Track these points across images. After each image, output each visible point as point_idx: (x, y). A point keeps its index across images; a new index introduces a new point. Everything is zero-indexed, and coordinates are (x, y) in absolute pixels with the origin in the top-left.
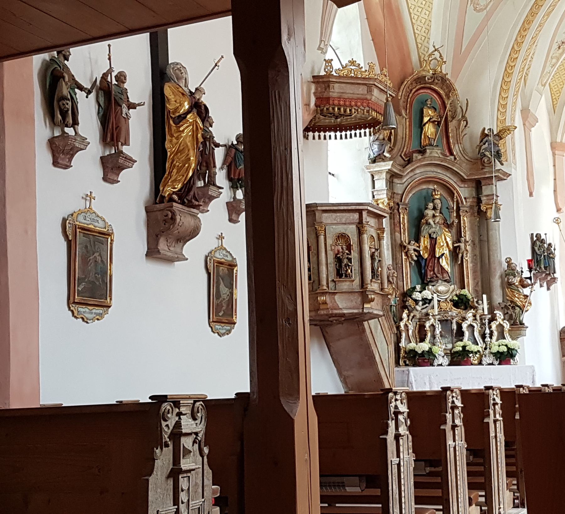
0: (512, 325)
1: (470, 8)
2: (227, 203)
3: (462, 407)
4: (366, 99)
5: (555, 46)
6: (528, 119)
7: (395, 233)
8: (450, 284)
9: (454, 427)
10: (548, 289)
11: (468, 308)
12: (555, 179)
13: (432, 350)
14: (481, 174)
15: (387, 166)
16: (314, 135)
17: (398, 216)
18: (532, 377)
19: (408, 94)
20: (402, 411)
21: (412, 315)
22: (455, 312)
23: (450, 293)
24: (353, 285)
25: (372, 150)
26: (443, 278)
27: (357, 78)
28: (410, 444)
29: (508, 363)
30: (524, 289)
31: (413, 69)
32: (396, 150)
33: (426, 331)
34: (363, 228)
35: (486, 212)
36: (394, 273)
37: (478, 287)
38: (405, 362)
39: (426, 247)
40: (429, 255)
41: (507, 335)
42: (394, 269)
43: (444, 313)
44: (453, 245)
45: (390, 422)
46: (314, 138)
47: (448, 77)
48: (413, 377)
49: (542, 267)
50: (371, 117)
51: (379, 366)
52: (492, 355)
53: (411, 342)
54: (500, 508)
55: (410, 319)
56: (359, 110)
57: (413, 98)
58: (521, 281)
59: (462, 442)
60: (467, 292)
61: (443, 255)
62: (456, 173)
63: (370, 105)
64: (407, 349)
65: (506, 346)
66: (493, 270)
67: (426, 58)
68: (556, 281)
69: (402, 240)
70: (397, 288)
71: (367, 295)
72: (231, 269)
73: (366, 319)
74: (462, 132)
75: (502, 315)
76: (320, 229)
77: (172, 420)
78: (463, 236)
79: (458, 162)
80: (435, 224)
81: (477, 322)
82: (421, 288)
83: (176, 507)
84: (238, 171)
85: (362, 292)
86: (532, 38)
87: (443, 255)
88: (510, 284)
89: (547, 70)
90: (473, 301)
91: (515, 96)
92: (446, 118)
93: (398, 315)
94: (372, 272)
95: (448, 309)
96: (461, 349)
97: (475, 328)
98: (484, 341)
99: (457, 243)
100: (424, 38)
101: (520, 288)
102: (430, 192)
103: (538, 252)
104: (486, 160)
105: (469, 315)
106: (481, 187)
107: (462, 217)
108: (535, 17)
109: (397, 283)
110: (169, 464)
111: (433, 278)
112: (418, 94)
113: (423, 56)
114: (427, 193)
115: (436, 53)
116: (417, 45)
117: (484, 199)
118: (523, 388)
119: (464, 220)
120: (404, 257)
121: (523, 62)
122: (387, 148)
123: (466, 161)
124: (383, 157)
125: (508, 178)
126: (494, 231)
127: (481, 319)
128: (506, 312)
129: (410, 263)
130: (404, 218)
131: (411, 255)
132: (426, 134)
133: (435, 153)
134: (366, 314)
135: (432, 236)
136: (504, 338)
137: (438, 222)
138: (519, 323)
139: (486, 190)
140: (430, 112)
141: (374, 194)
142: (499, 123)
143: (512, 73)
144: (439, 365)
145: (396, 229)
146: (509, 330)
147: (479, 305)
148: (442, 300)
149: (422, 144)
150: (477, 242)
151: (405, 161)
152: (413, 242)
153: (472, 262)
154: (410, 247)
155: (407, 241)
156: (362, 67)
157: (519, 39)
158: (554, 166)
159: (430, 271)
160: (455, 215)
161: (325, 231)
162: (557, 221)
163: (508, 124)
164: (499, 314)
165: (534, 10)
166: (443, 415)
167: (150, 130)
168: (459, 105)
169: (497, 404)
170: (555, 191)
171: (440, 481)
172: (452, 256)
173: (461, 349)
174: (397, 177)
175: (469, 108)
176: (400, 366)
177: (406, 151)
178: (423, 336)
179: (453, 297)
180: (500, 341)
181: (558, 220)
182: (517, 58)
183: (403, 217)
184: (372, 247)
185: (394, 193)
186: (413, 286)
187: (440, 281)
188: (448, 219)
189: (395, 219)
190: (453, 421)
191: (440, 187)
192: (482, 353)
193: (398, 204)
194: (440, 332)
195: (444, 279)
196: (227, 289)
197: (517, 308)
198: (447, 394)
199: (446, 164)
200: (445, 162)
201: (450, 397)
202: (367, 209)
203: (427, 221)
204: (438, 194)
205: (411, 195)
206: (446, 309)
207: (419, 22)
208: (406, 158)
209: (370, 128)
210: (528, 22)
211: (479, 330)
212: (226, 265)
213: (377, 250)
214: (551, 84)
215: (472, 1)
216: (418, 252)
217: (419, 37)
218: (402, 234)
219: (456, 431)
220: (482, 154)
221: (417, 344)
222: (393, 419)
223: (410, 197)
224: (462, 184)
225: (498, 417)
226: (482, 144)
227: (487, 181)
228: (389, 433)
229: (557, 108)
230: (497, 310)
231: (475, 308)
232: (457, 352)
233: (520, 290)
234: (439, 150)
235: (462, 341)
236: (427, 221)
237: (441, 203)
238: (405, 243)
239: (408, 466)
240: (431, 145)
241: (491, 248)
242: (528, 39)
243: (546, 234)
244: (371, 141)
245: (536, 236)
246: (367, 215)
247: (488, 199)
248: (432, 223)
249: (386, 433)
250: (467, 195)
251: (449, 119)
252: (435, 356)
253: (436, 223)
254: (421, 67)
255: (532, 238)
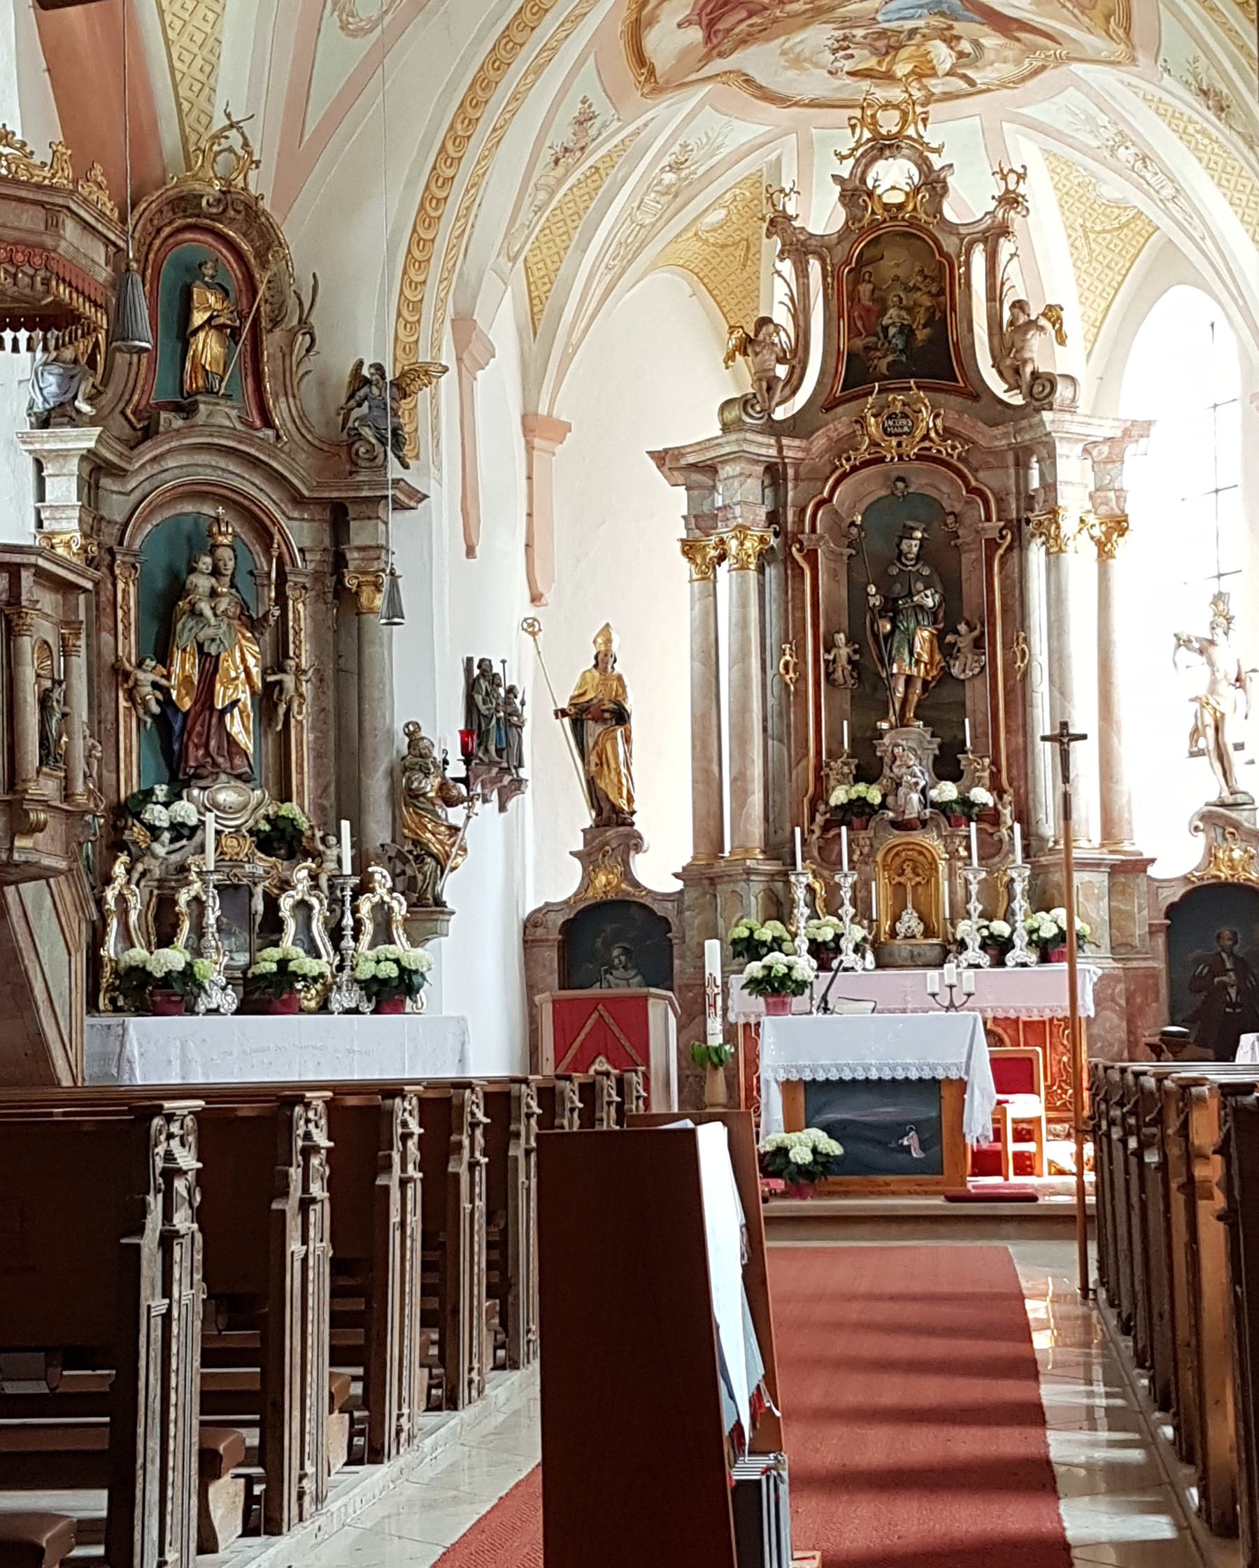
0: (414, 905)
1: (331, 21)
4: (44, 248)
5: (546, 156)
7: (99, 630)
8: (251, 785)
9: (306, 1204)
10: (502, 808)
11: (299, 856)
12: (530, 515)
13: (196, 969)
14: (349, 487)
15: (85, 439)
17: (110, 586)
18: (458, 1047)
19: (149, 240)
20: (185, 1168)
21: (140, 867)
22: (261, 864)
23: (249, 812)
25: (41, 389)
26: (232, 768)
27: (16, 182)
28: (199, 1257)
29: (398, 1009)
30: (449, 810)
31: (164, 171)
32: (109, 394)
33: (177, 915)
34: (20, 617)
35: (357, 593)
36: (94, 747)
38: (113, 1001)
39: (187, 679)
40: (195, 704)
41: (398, 933)
42: (92, 736)
43: (233, 867)
44: (263, 680)
45: (150, 1198)
47: (266, 205)
48: (135, 1044)
49: (492, 749)
50: (50, 299)
51: (41, 1012)
52: (356, 987)
53: (133, 946)
54: (400, 1416)
55: (134, 880)
56: (20, 275)
57: (161, 255)
58: (443, 787)
59: (324, 1244)
60: (297, 810)
61: (235, 703)
62: (277, 479)
63: (53, 264)
64: (122, 965)
65: (397, 961)
66: (369, 752)
67: (204, 144)
68: (523, 788)
69: (120, 654)
70: (100, 790)
71: (26, 813)
73: (12, 878)
74: (298, 364)
75: (389, 878)
78: (291, 654)
79: (286, 448)
80: (215, 615)
81: (322, 895)
82: (168, 794)
85: (9, 803)
86: (495, 130)
88: (414, 796)
89: (525, 215)
90: (314, 835)
91: (445, 283)
92: (256, 321)
93: (98, 866)
94: (41, 745)
95: (242, 856)
96: (274, 967)
97: (316, 911)
98: (337, 948)
99: (274, 673)
100: (200, 85)
101: (441, 807)
102: (204, 524)
103: (483, 708)
104: (362, 450)
105: (301, 875)
106: (348, 524)
107: (291, 602)
108: (505, 72)
109: (100, 776)
111: (204, 766)
112: (178, 244)
113: (193, 138)
114: (196, 524)
116: (179, 105)
117: (353, 557)
118: (473, 1090)
119: (296, 611)
120: (123, 703)
121: (467, 191)
122: (85, 388)
124: (74, 414)
125: (420, 505)
126: (377, 648)
127: (331, 887)
128: (398, 871)
129: (139, 719)
130: (128, 593)
131: (143, 699)
132: (197, 361)
134: (17, 866)
135: (206, 650)
136: (392, 942)
137: (225, 612)
138: (431, 902)
139: (360, 534)
140: (212, 300)
141: (43, 516)
142: (399, 353)
143: (439, 218)
144: (209, 1012)
145: (103, 619)
146: (406, 920)
147: (328, 847)
148: (227, 830)
149: (187, 386)
150: (329, 673)
151: (134, 428)
152: (150, 663)
153: (313, 728)
154: (141, 675)
155: (133, 659)
156: (32, 153)
157: (459, 126)
158: (529, 478)
159: (197, 747)
160: (273, 594)
162: (531, 627)
163: (424, 357)
164: (380, 875)
165: (503, 53)
166: (279, 1172)
168: (293, 288)
169: (411, 1135)
170: (527, 545)
171: (258, 1345)
172: (260, 709)
173: (274, 967)
174: (110, 474)
175: (318, 299)
176: (98, 1011)
177: (139, 401)
178: (168, 930)
179: (257, 822)
180: (380, 947)
181: (533, 625)
182: (453, 178)
183: (124, 591)
184: (42, 672)
185: (102, 518)
186: (143, 788)
187: (223, 777)
189: (102, 593)
190: (306, 1189)
191: (232, 513)
192: (330, 979)
193: (111, 552)
194: (218, 919)
195: (235, 772)
197: (429, 860)
198: (295, 1114)
199: (252, 451)
200: (252, 446)
201: (302, 1122)
202: (36, 566)
205: (150, 527)
206: (238, 854)
207: (185, 40)
208: (139, 421)
209: (46, 331)
210: (483, 85)
211: (325, 917)
213: (60, 683)
214: (531, 260)
215: (335, 4)
216: (166, 691)
217: (187, 82)
218: (121, 638)
219: (312, 1214)
220: (353, 433)
221: (151, 953)
222: (159, 1191)
223: (146, 531)
224: (294, 509)
225: (411, 1171)
226: (352, 403)
228: (148, 1231)
229: (542, 322)
230: (377, 864)
231: (317, 856)
232: (263, 977)
233: (439, 811)
234: (233, 408)
235: (276, 944)
236: (193, 605)
237: (236, 557)
238: (127, 666)
239: (190, 1319)
240: (212, 392)
241: (367, 693)
242: (482, 132)
243: (504, 662)
244: (38, 362)
245: (479, 667)
246: (35, 582)
247: (363, 559)
248: (208, 612)
249: (140, 1230)
250: (307, 543)
251: (263, 324)
252: (201, 987)
253: (218, 612)
254: (189, 168)
255: (468, 670)
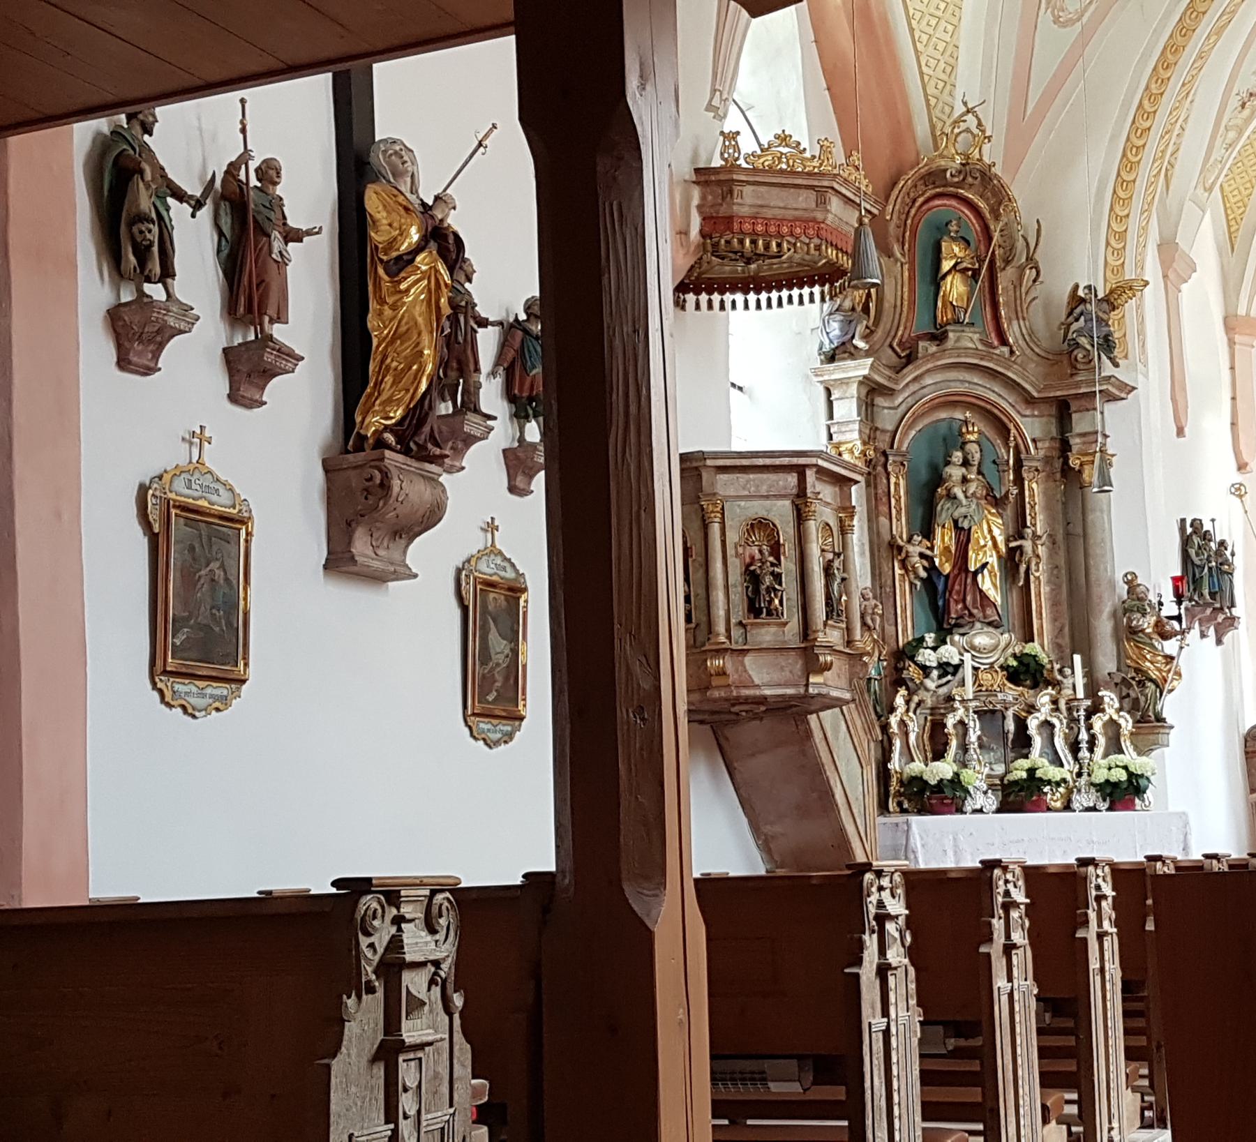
0: (1139, 722)
1: (1045, 17)
2: (504, 451)
3: (1026, 905)
4: (814, 220)
5: (1234, 102)
6: (1175, 265)
7: (877, 517)
8: (1000, 630)
9: (1009, 948)
10: (1219, 642)
11: (1041, 685)
12: (1233, 399)
13: (961, 778)
14: (1069, 387)
15: (860, 368)
16: (697, 300)
17: (885, 481)
18: (1182, 837)
19: (907, 209)
20: (893, 914)
21: (916, 699)
22: (1011, 692)
23: (999, 652)
24: (784, 632)
25: (827, 333)
26: (985, 618)
27: (794, 173)
28: (913, 986)
29: (1129, 806)
30: (1165, 643)
31: (918, 154)
32: (879, 333)
33: (946, 735)
34: (806, 506)
35: (1080, 472)
36: (876, 606)
37: (1063, 637)
38: (900, 804)
39: (947, 549)
40: (954, 567)
41: (1126, 744)
42: (875, 598)
43: (988, 696)
44: (1007, 545)
45: (866, 937)
46: (698, 307)
47: (997, 170)
48: (917, 837)
49: (1206, 592)
50: (824, 261)
51: (842, 813)
52: (1093, 790)
53: (913, 760)
54: (1110, 1129)
55: (912, 710)
56: (798, 244)
57: (917, 218)
58: (1159, 624)
59: (1028, 983)
60: (1038, 648)
61: (984, 565)
62: (1013, 385)
63: (823, 233)
64: (905, 776)
65: (1126, 768)
66: (1095, 599)
67: (948, 130)
68: (1236, 624)
69: (894, 532)
70: (883, 640)
71: (817, 655)
72: (514, 598)
73: (813, 708)
74: (1027, 293)
75: (1116, 700)
76: (711, 508)
77: (383, 934)
78: (1028, 524)
79: (1019, 361)
80: (966, 497)
81: (1061, 716)
82: (936, 640)
83: (392, 1126)
84: (528, 380)
85: (805, 648)
86: (1183, 85)
87: (984, 565)
88: (1133, 632)
89: (1215, 155)
90: (1053, 668)
91: (1146, 214)
92: (992, 262)
93: (884, 699)
94: (827, 604)
95: (995, 687)
96: (1024, 775)
97: (1057, 730)
98: (1076, 759)
99: (1016, 540)
100: (942, 84)
101: (1157, 640)
102: (956, 425)
103: (1196, 560)
104: (1080, 356)
105: (1044, 699)
106: (1070, 416)
107: (1026, 483)
108: (1190, 37)
109: (883, 629)
110: (375, 1031)
111: (962, 617)
112: (929, 209)
113: (939, 125)
114: (950, 428)
115: (970, 117)
116: (927, 101)
117: (1075, 442)
118: (1164, 862)
119: (1031, 489)
120: (898, 571)
121: (1162, 137)
122: (860, 329)
123: (1035, 358)
124: (852, 350)
125: (1129, 396)
126: (1098, 514)
127: (1069, 709)
128: (1124, 694)
129: (911, 584)
130: (899, 485)
131: (913, 567)
132: (946, 298)
133: (967, 340)
134: (813, 697)
135: (960, 525)
136: (1121, 751)
137: (974, 494)
138: (1153, 718)
139: (1080, 423)
140: (956, 249)
141: (832, 431)
142: (1109, 274)
143: (1139, 162)
144: (975, 811)
145: (880, 508)
146: (1132, 734)
147: (1065, 677)
148: (982, 667)
149: (939, 320)
150: (1060, 537)
151: (899, 357)
152: (917, 538)
153: (1049, 582)
154: (911, 548)
155: (905, 536)
156: (805, 149)
157: (1153, 86)
158: (1232, 368)
159: (957, 602)
160: (1011, 477)
161: (723, 514)
162: (1238, 491)
163: (1129, 275)
164: (1109, 698)
165: (1188, 21)
166: (984, 921)
167: (335, 290)
168: (1020, 233)
169: (1105, 897)
170: (1233, 424)
172: (1005, 568)
173: (1024, 775)
174: (882, 394)
175: (1042, 239)
176: (889, 812)
177: (902, 336)
178: (941, 747)
179: (1006, 659)
180: (1111, 757)
181: (1239, 489)
182: (1149, 129)
183: (895, 483)
184: (826, 548)
185: (877, 429)
186: (917, 636)
187: (978, 625)
188: (995, 486)
189: (879, 487)
190: (1008, 936)
191: (977, 416)
192: (1071, 784)
193: (885, 454)
194: (979, 738)
195: (987, 621)
196: (505, 642)
197: (1149, 684)
198: (994, 876)
199: (991, 365)
200: (989, 361)
201: (1001, 883)
202: (816, 465)
203: (949, 490)
204: (973, 432)
205: (914, 432)
206: (992, 685)
207: (931, 48)
208: (903, 350)
209: (822, 285)
210: (1173, 49)
211: (1065, 734)
212: (501, 588)
213: (838, 555)
214: (1225, 186)
215: (1048, 3)
216: (930, 559)
217: (932, 83)
218: (894, 520)
219: (1014, 958)
220: (1072, 343)
221: (927, 765)
222: (873, 932)
223: (911, 437)
224: (1027, 408)
225: (1106, 925)
226: (1071, 319)
227: (1083, 402)
228: (866, 963)
229: (1238, 239)
230: (1106, 689)
231: (1056, 684)
232: (1016, 783)
233: (1156, 644)
234: (975, 333)
235: (1026, 757)
236: (949, 490)
237: (981, 451)
238: (899, 541)
239: (908, 1036)
240: (959, 322)
241: (1091, 551)
242: (1174, 87)
243: (1213, 520)
244: (825, 312)
245: (1192, 525)
246: (817, 478)
247: (1084, 443)
248: (960, 495)
249: (859, 962)
250: (1037, 434)
251: (998, 264)
252: (967, 791)
253: (969, 495)
254: (936, 148)
255: (1182, 528)
